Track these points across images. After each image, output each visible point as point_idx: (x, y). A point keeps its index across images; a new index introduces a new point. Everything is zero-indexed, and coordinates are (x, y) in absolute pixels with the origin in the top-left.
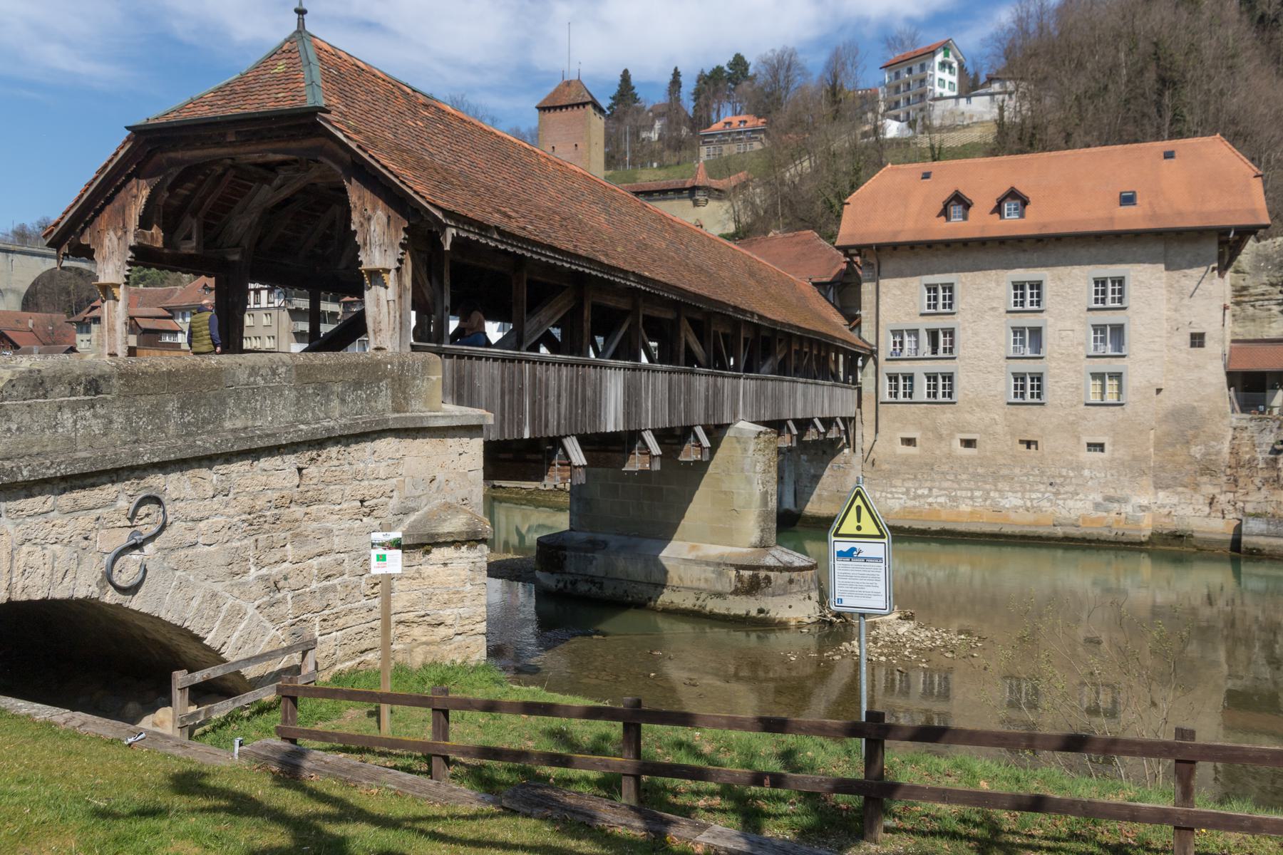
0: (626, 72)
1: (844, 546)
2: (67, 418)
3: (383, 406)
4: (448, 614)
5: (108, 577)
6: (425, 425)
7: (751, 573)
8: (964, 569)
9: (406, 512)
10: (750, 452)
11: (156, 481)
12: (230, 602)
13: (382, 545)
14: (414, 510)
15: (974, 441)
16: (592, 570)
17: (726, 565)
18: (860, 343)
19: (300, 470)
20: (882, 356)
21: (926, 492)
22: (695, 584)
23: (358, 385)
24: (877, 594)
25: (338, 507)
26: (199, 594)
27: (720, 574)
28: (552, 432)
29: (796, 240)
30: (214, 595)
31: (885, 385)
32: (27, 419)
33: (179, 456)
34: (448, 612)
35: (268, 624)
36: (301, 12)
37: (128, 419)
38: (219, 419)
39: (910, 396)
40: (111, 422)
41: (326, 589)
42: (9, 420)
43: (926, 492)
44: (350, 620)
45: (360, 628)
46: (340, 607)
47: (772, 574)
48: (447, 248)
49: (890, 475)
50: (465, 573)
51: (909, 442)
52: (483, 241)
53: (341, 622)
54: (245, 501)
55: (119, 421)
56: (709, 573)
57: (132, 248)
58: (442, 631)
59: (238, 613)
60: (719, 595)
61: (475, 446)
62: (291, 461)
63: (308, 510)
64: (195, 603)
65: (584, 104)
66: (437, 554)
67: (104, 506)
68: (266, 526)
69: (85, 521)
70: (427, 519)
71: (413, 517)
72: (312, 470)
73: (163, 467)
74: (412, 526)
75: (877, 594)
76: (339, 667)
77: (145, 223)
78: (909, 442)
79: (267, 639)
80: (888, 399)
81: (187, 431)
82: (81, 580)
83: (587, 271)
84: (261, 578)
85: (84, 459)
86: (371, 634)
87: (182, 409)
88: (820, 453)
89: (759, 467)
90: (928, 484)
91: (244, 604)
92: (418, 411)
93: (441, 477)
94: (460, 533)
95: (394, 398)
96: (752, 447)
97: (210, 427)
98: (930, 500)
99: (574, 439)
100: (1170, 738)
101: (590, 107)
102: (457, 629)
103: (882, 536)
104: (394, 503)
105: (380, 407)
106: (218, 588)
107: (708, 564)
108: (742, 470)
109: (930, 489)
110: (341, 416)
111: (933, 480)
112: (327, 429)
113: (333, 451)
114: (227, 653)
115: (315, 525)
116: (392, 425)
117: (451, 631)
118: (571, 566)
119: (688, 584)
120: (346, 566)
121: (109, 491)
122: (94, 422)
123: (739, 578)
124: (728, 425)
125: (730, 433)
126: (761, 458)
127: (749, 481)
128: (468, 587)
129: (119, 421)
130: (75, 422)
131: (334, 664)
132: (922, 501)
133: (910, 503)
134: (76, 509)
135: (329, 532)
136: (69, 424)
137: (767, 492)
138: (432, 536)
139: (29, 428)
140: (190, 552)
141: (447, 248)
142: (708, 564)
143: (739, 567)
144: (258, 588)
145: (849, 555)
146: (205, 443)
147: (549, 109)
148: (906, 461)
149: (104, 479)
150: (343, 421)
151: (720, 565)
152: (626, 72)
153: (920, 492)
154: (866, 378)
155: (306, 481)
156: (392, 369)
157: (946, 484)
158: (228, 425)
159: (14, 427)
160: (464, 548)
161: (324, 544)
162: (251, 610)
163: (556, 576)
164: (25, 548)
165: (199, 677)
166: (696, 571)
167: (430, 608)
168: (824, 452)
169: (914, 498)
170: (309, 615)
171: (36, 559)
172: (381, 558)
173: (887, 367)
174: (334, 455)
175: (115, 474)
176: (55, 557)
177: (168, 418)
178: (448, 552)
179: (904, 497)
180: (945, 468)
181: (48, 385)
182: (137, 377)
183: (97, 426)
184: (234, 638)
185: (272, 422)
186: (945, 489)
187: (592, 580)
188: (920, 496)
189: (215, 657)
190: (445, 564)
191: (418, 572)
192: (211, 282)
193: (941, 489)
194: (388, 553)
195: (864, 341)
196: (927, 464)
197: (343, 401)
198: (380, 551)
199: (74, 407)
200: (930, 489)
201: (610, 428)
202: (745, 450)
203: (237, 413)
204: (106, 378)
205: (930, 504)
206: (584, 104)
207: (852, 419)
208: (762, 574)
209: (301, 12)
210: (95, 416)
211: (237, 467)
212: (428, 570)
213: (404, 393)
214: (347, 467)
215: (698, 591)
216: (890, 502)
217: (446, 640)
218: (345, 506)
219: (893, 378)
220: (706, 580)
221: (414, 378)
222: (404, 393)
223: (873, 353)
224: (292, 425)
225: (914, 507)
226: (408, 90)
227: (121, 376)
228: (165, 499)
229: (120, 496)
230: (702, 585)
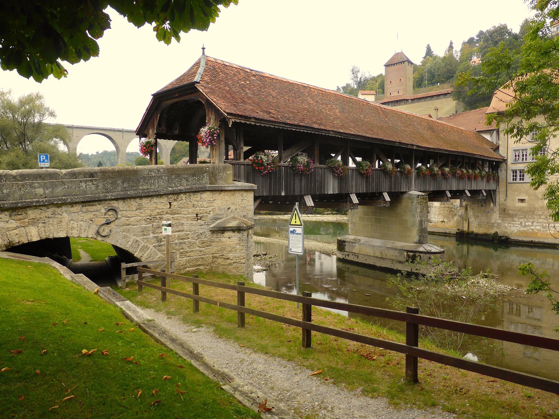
0: (429, 45)
1: (291, 229)
2: (83, 185)
3: (205, 181)
4: (231, 255)
5: (98, 233)
6: (223, 189)
7: (413, 254)
8: (550, 260)
9: (217, 219)
10: (415, 203)
11: (115, 204)
12: (143, 244)
13: (165, 225)
14: (220, 219)
15: (525, 200)
16: (354, 251)
17: (403, 250)
18: (500, 158)
19: (170, 203)
20: (510, 161)
21: (530, 224)
22: (391, 257)
23: (194, 175)
24: (300, 247)
25: (186, 216)
26: (131, 240)
27: (401, 254)
28: (297, 193)
29: (479, 112)
30: (137, 241)
31: (510, 174)
32: (70, 185)
33: (121, 197)
34: (231, 254)
35: (158, 252)
36: (203, 49)
37: (104, 185)
38: (137, 186)
39: (523, 180)
40: (98, 186)
41: (181, 243)
42: (65, 185)
43: (530, 224)
44: (192, 254)
45: (197, 257)
46: (188, 249)
47: (421, 255)
48: (230, 126)
49: (512, 216)
50: (237, 242)
51: (522, 201)
52: (248, 123)
53: (188, 254)
54: (148, 212)
55: (101, 186)
56: (396, 253)
57: (155, 134)
58: (229, 261)
59: (147, 248)
60: (400, 262)
61: (251, 196)
62: (164, 200)
63: (173, 216)
64: (130, 243)
65: (404, 62)
66: (227, 234)
67: (97, 211)
68: (157, 221)
69: (90, 215)
70: (224, 221)
71: (219, 221)
72: (174, 203)
73: (116, 199)
74: (217, 224)
75: (300, 247)
76: (187, 269)
77: (159, 125)
78: (522, 201)
79: (158, 257)
80: (512, 181)
81: (125, 189)
82: (90, 232)
83: (313, 132)
84: (155, 237)
85: (88, 197)
86: (201, 260)
87: (123, 182)
88: (480, 206)
89: (418, 210)
90: (531, 220)
91: (149, 245)
92: (221, 184)
93: (233, 207)
94: (234, 227)
95: (210, 179)
96: (415, 201)
97: (134, 188)
98: (532, 228)
99: (310, 196)
100: (404, 312)
101: (407, 63)
102: (234, 261)
103: (301, 225)
104: (211, 215)
105: (204, 182)
106: (138, 239)
107: (396, 249)
108: (411, 211)
109: (533, 223)
110: (187, 185)
111: (534, 218)
112: (179, 190)
113: (183, 196)
114: (143, 259)
115: (176, 221)
116: (207, 189)
117: (232, 261)
118: (347, 248)
119: (388, 257)
120: (190, 236)
121: (98, 207)
122: (92, 186)
123: (408, 256)
124: (405, 192)
125: (405, 196)
126: (419, 206)
127: (414, 216)
128: (238, 246)
129: (101, 186)
130: (86, 186)
131: (186, 268)
132: (528, 228)
133: (522, 229)
134: (88, 211)
135: (182, 224)
136: (84, 186)
137: (422, 220)
138: (224, 227)
139: (71, 187)
140: (128, 227)
141: (230, 126)
142: (396, 249)
143: (408, 251)
144: (154, 240)
145: (293, 232)
146: (131, 193)
147: (389, 65)
148: (520, 210)
149: (96, 203)
150: (187, 187)
151: (401, 250)
152: (429, 45)
153: (527, 224)
154: (501, 174)
155: (172, 207)
156: (209, 170)
157: (540, 220)
158: (141, 188)
159: (66, 187)
160: (236, 233)
161: (180, 228)
162: (151, 247)
163: (343, 253)
164: (71, 222)
165: (129, 265)
166: (392, 252)
167: (224, 253)
168: (482, 206)
169: (525, 227)
170: (175, 251)
171: (75, 225)
172: (165, 229)
173: (511, 166)
174: (184, 198)
175: (100, 201)
176: (81, 225)
177: (118, 185)
178: (230, 234)
179: (519, 226)
180: (540, 213)
181: (77, 175)
182: (107, 172)
183: (93, 188)
184: (145, 255)
185: (158, 187)
186: (539, 223)
187: (354, 254)
188: (527, 226)
189: (136, 260)
190: (229, 238)
191: (220, 240)
192: (188, 143)
193: (538, 223)
194: (167, 228)
195: (501, 155)
196: (531, 211)
197: (187, 180)
198: (165, 227)
199: (86, 182)
200: (533, 223)
201: (331, 192)
202: (412, 203)
203: (144, 184)
204: (96, 173)
205: (532, 229)
206: (404, 62)
207: (494, 191)
208: (417, 254)
209: (203, 49)
210: (93, 184)
211: (145, 201)
212: (223, 239)
213: (215, 177)
214: (189, 203)
215: (393, 260)
216: (513, 228)
217: (230, 264)
218: (189, 216)
219: (515, 172)
220: (395, 256)
221: (219, 173)
222: (215, 177)
223: (505, 161)
224: (166, 188)
225: (524, 230)
226: (248, 70)
227: (101, 172)
228: (118, 210)
229: (102, 208)
230: (394, 258)
